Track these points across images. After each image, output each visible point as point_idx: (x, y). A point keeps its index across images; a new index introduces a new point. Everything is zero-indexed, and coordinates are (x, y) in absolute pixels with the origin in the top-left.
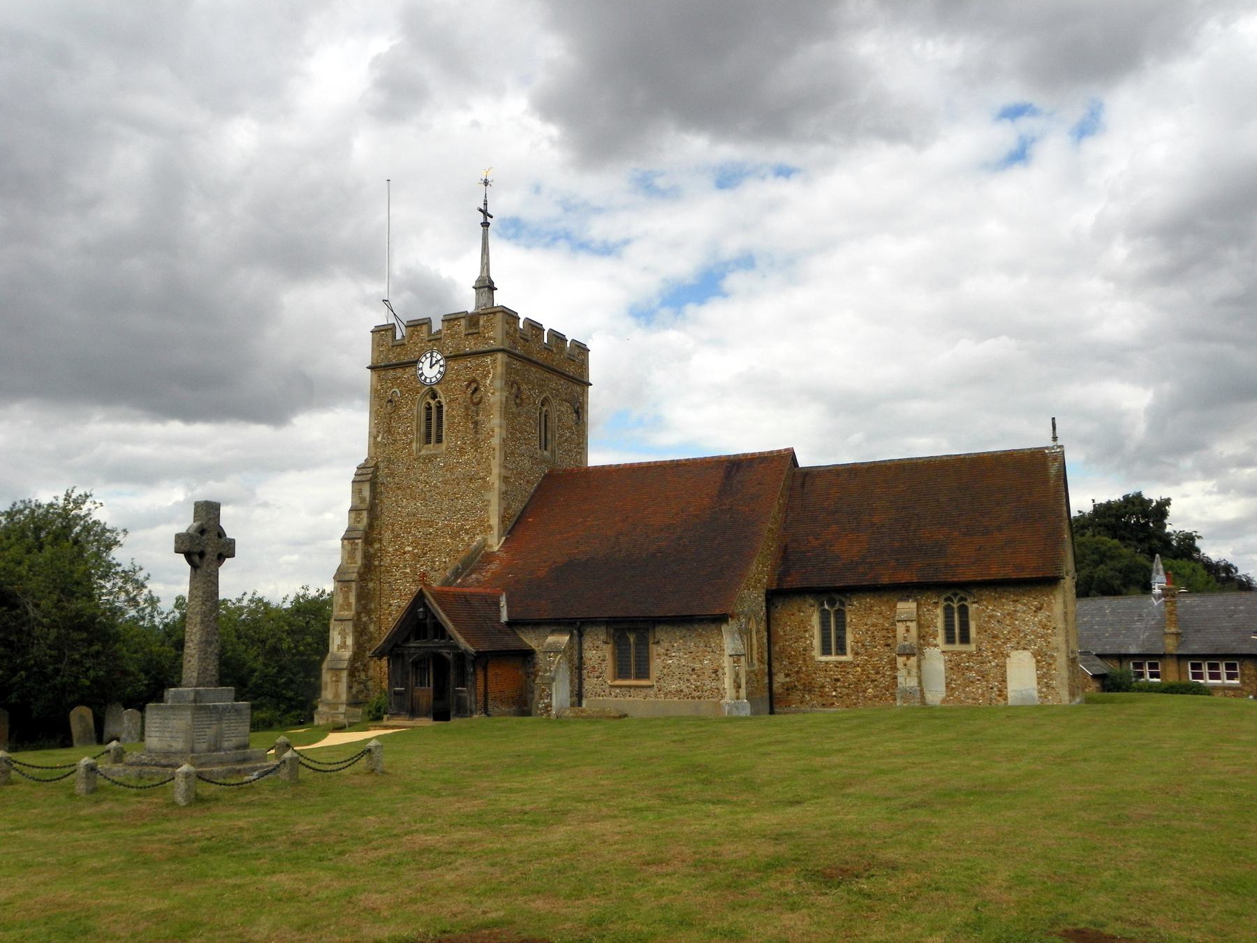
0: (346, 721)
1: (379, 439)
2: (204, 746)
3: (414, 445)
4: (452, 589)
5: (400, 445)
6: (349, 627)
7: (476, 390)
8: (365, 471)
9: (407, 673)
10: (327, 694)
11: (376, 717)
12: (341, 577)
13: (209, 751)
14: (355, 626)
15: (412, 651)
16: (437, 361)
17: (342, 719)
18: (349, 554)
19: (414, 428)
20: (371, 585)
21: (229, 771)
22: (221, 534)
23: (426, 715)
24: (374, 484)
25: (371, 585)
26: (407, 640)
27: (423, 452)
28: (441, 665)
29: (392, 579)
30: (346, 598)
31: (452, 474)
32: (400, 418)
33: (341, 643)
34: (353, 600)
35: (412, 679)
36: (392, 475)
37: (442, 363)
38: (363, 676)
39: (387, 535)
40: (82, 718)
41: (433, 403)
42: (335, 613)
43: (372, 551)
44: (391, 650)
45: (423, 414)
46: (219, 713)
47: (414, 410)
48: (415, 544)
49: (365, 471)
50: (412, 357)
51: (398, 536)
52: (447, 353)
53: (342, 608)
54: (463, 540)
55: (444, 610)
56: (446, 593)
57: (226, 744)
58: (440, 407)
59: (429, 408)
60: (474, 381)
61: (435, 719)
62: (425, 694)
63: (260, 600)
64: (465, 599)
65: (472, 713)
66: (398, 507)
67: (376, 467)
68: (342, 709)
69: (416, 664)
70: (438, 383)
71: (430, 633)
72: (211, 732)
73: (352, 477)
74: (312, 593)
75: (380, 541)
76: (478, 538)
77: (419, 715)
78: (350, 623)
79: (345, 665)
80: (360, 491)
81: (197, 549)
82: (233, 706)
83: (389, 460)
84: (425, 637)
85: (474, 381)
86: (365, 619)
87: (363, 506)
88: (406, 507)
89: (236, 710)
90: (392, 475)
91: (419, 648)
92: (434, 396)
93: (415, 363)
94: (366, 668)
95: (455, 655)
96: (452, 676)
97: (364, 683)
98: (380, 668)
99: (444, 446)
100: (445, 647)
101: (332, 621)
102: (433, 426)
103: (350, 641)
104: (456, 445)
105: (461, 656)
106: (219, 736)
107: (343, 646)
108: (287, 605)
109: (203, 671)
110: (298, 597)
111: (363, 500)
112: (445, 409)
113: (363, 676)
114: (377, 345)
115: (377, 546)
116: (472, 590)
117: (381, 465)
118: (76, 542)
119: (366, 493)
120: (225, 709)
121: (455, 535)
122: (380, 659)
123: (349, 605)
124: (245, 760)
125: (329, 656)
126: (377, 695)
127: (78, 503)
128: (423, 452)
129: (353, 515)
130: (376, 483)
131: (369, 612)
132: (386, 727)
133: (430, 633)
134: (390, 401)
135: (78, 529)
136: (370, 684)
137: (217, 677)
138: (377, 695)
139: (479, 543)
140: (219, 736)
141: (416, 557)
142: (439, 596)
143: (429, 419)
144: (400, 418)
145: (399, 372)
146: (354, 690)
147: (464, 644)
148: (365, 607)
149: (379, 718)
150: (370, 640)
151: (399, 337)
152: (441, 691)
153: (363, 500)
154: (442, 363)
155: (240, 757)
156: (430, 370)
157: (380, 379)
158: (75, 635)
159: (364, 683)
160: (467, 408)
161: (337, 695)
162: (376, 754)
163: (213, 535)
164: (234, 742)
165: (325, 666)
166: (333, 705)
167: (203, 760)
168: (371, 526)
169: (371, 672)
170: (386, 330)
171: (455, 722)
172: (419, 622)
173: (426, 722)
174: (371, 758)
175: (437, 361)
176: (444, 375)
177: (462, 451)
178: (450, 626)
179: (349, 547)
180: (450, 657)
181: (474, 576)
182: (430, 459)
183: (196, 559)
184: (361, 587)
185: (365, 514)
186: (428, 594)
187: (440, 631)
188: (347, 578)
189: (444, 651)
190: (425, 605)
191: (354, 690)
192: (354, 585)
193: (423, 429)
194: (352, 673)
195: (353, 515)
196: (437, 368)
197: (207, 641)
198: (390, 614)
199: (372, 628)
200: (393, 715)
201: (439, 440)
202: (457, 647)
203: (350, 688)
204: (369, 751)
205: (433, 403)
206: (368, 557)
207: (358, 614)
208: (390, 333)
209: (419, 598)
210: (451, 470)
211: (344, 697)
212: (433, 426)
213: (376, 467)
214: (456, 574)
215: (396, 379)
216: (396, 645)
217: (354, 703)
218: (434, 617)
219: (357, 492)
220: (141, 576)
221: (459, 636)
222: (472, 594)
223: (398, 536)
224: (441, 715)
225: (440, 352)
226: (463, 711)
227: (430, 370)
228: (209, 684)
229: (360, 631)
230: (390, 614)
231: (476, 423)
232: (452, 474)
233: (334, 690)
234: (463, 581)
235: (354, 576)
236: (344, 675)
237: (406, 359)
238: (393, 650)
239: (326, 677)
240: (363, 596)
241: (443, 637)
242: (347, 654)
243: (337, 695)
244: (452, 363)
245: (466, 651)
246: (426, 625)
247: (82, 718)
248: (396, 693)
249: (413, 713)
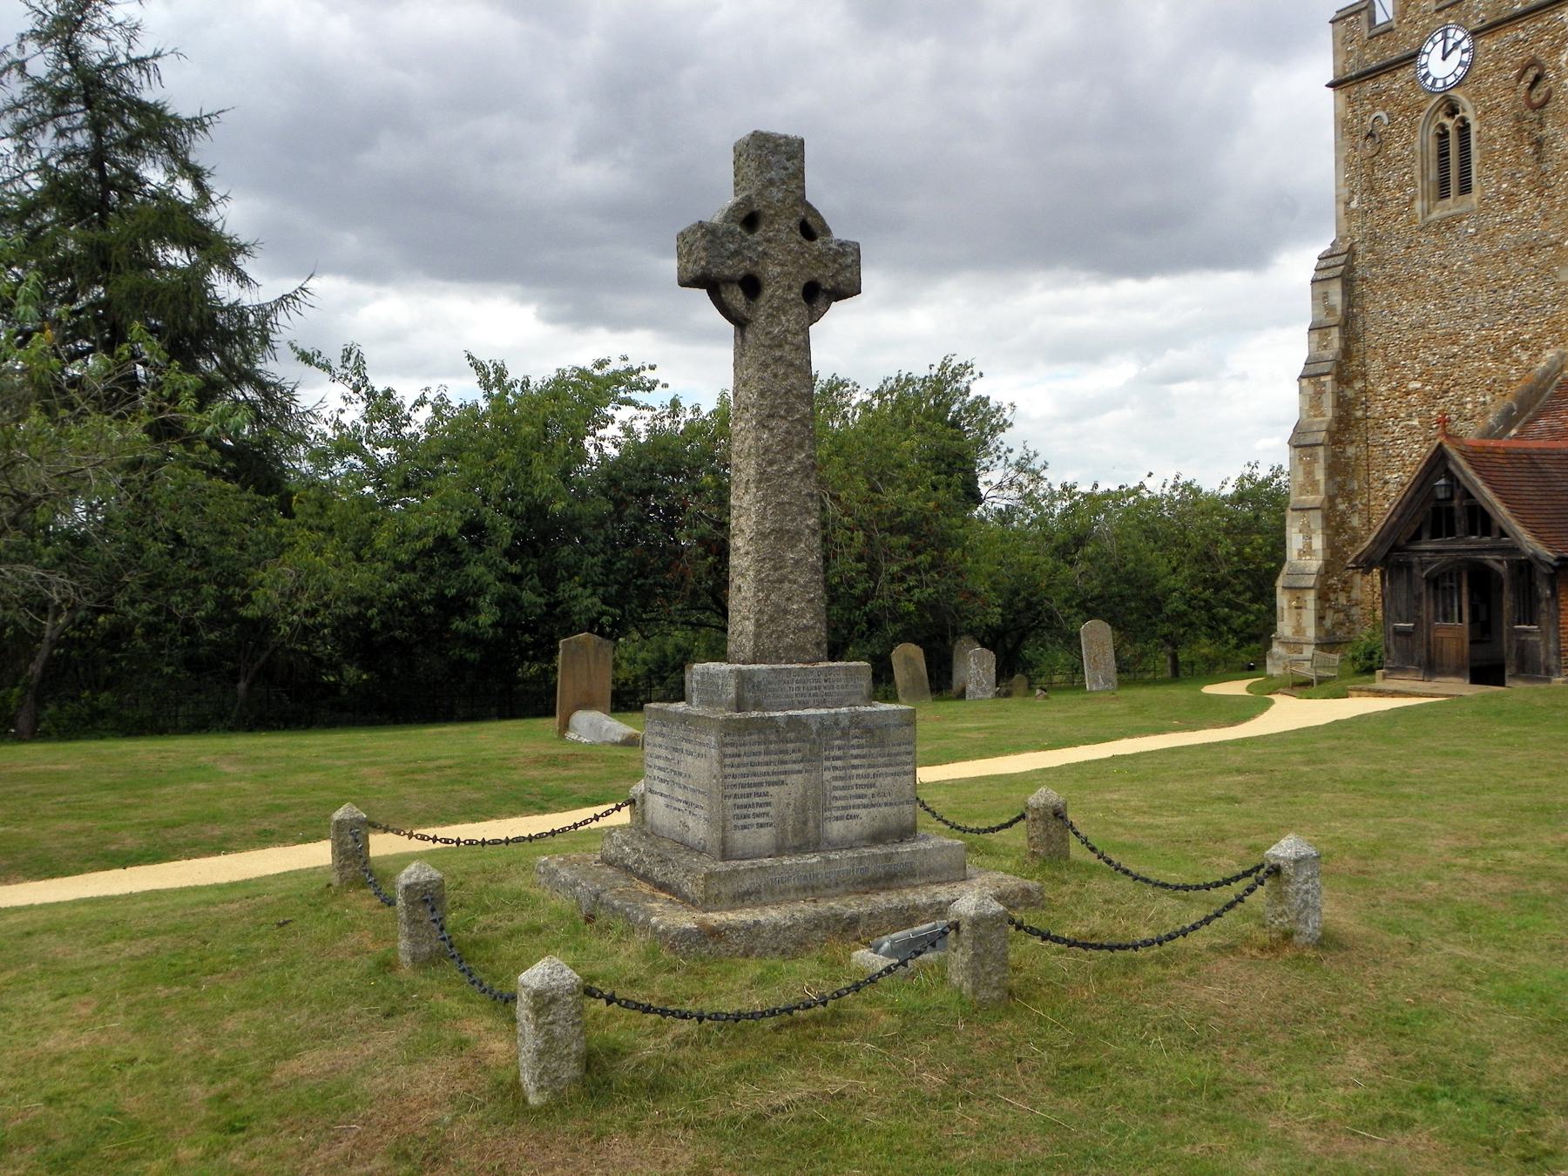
0: (1312, 675)
1: (1354, 205)
2: (765, 837)
3: (1418, 205)
4: (1504, 443)
5: (1392, 208)
6: (1316, 521)
7: (1538, 79)
8: (1331, 262)
9: (1419, 598)
10: (1285, 628)
11: (1365, 668)
12: (1300, 442)
13: (780, 850)
14: (1326, 519)
15: (1427, 557)
16: (1456, 46)
17: (1306, 670)
18: (1313, 401)
19: (1417, 173)
20: (1351, 451)
21: (817, 923)
22: (810, 228)
23: (1457, 673)
24: (1348, 281)
25: (1351, 451)
26: (1417, 537)
27: (1435, 215)
28: (1482, 582)
29: (1388, 438)
30: (1309, 473)
31: (1493, 244)
32: (1389, 160)
33: (1305, 547)
34: (1320, 476)
35: (1427, 608)
36: (1380, 262)
37: (1465, 45)
38: (1343, 600)
39: (1376, 366)
40: (909, 660)
41: (1450, 123)
42: (1293, 499)
43: (1350, 393)
44: (1386, 557)
45: (1433, 147)
46: (811, 742)
47: (1415, 145)
48: (1426, 375)
49: (1331, 262)
50: (1407, 49)
51: (1395, 365)
52: (1475, 24)
53: (1303, 490)
54: (1518, 361)
55: (1488, 482)
56: (1493, 451)
57: (836, 829)
58: (1464, 129)
59: (1443, 135)
60: (1533, 63)
61: (1475, 680)
62: (1454, 634)
63: (1188, 485)
64: (1530, 461)
65: (1549, 672)
66: (1393, 316)
67: (1351, 252)
68: (1308, 651)
69: (1434, 581)
70: (1459, 84)
71: (1461, 525)
72: (789, 791)
73: (1311, 274)
74: (1262, 473)
75: (1364, 376)
76: (1549, 354)
77: (1443, 674)
78: (1319, 513)
79: (1311, 581)
80: (1326, 296)
81: (733, 268)
82: (856, 720)
83: (1374, 238)
84: (1451, 532)
85: (1533, 63)
86: (1342, 507)
87: (1331, 320)
88: (1408, 313)
89: (869, 731)
90: (1380, 262)
91: (1438, 551)
92: (1452, 110)
93: (1414, 57)
94: (1347, 586)
95: (1511, 564)
96: (1508, 601)
97: (1345, 611)
98: (1368, 588)
99: (1474, 197)
100: (1491, 550)
101: (1289, 511)
102: (1452, 166)
103: (1318, 543)
104: (1498, 192)
105: (1525, 568)
106: (814, 806)
107: (1307, 551)
108: (1229, 490)
109: (771, 618)
110: (1242, 479)
111: (1330, 310)
112: (1474, 128)
113: (1343, 600)
114: (1342, 45)
115: (1358, 385)
116: (1542, 444)
117: (1360, 248)
118: (955, 424)
119: (1336, 298)
120: (828, 727)
121: (1502, 353)
122: (1367, 571)
123: (1314, 483)
124: (889, 879)
125: (1286, 568)
126: (1368, 630)
127: (956, 375)
128: (1435, 215)
129: (1316, 336)
130: (1352, 280)
131: (1349, 496)
132: (1380, 693)
133: (1461, 525)
134: (1371, 135)
135: (955, 408)
136: (1356, 612)
137: (821, 632)
138: (1368, 630)
139: (1552, 363)
140: (814, 806)
141: (1429, 399)
142: (1476, 457)
143: (1443, 154)
144: (1389, 160)
145: (1384, 81)
146: (1328, 623)
147: (1530, 543)
148: (1341, 487)
149: (1370, 671)
150: (1352, 542)
151: (1381, 18)
152: (1484, 627)
153: (1330, 310)
154: (1465, 45)
155: (873, 869)
156: (1441, 65)
157: (1350, 102)
158: (893, 541)
159: (1345, 611)
160: (1519, 119)
161: (1299, 630)
162: (1299, 883)
163: (783, 229)
164: (866, 819)
165: (1280, 583)
166: (1295, 645)
167: (747, 884)
168: (1346, 352)
169: (1356, 594)
170: (1358, 12)
171: (1516, 691)
172: (1439, 504)
173: (1460, 687)
174: (1281, 897)
175: (1456, 46)
176: (1470, 66)
177: (1511, 201)
178: (1501, 512)
179: (1310, 390)
180: (1502, 569)
181: (1542, 422)
182: (1449, 224)
183: (736, 297)
184: (1334, 455)
185: (1335, 333)
186: (1453, 453)
187: (1481, 520)
188: (1309, 440)
189: (1490, 559)
190: (1449, 474)
191: (1328, 623)
192: (1321, 451)
193: (1433, 174)
194: (1323, 597)
195: (1316, 336)
196: (1455, 57)
197: (779, 533)
198: (1386, 497)
199: (1355, 521)
200: (1394, 671)
201: (1465, 188)
202: (1515, 550)
203: (1320, 618)
204: (1276, 871)
205: (1450, 123)
206: (1342, 403)
207: (1331, 499)
208: (1364, 16)
209: (1438, 461)
210: (1491, 239)
211: (1311, 633)
212: (1452, 166)
213: (1351, 252)
214: (1508, 419)
215: (1379, 95)
216: (1395, 548)
217: (1327, 643)
218: (1469, 495)
219: (1321, 298)
220: (1036, 464)
221: (1519, 529)
222: (1542, 452)
223: (1395, 365)
224: (1486, 672)
225: (1459, 25)
226: (1530, 668)
227: (1441, 65)
228: (796, 652)
229: (1335, 526)
230: (1386, 497)
231: (1539, 144)
232: (1493, 244)
233: (1296, 620)
234: (1521, 432)
235: (1321, 437)
236: (1311, 597)
237: (1397, 55)
238: (1391, 556)
239: (1283, 600)
240: (1337, 468)
241: (1487, 531)
242: (1315, 564)
243: (1299, 630)
244: (1491, 43)
245: (1536, 556)
246: (1451, 510)
247: (909, 660)
248: (1399, 633)
249: (1432, 667)
